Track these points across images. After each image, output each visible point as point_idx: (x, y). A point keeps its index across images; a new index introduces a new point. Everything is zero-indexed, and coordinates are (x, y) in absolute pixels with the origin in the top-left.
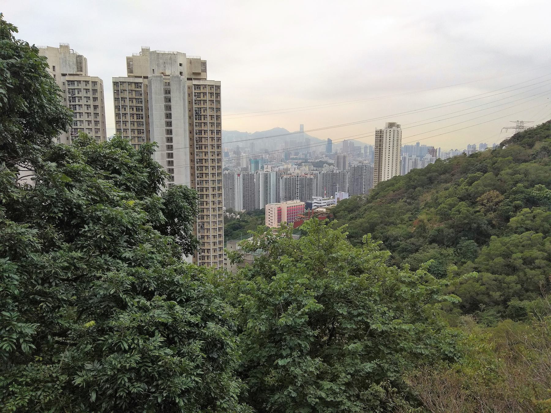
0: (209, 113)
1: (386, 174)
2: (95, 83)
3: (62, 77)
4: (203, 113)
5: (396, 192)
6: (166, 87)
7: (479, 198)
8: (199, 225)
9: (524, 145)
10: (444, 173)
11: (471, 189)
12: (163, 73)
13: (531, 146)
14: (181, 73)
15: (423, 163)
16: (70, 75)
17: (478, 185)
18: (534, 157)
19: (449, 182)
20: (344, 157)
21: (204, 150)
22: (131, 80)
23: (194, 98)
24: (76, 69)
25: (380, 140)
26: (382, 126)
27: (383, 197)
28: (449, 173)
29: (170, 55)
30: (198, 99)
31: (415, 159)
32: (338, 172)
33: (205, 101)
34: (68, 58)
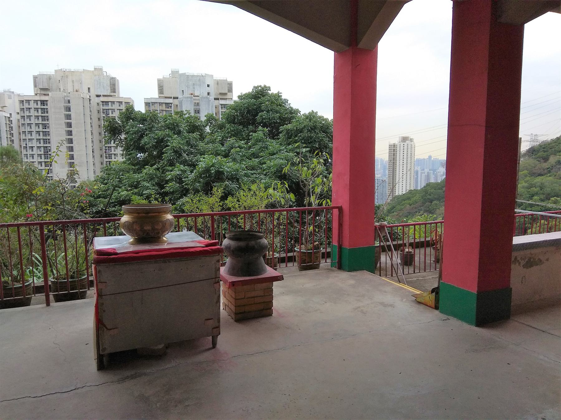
1: (401, 188)
3: (97, 98)
5: (412, 206)
6: (196, 107)
9: (539, 159)
12: (192, 94)
13: (546, 159)
14: (208, 94)
15: (436, 177)
16: (104, 96)
18: (549, 171)
22: (163, 101)
24: (109, 91)
25: (394, 154)
26: (396, 141)
27: (399, 210)
31: (428, 173)
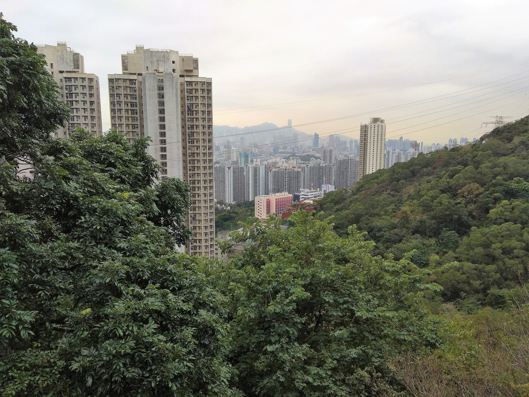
0: (200, 108)
1: (371, 167)
2: (91, 80)
3: (60, 74)
4: (194, 109)
5: (380, 185)
6: (159, 84)
7: (460, 191)
8: (191, 216)
9: (503, 140)
10: (426, 167)
11: (453, 182)
12: (156, 70)
13: (510, 140)
14: (174, 70)
15: (406, 157)
16: (67, 72)
17: (459, 178)
18: (513, 151)
19: (431, 175)
20: (331, 151)
21: (195, 144)
22: (126, 77)
23: (186, 94)
24: (73, 67)
25: (365, 135)
26: (367, 121)
27: (368, 189)
28: (431, 166)
29: (163, 53)
30: (190, 95)
31: (399, 153)
32: (324, 165)
33: (197, 97)
34: (65, 56)
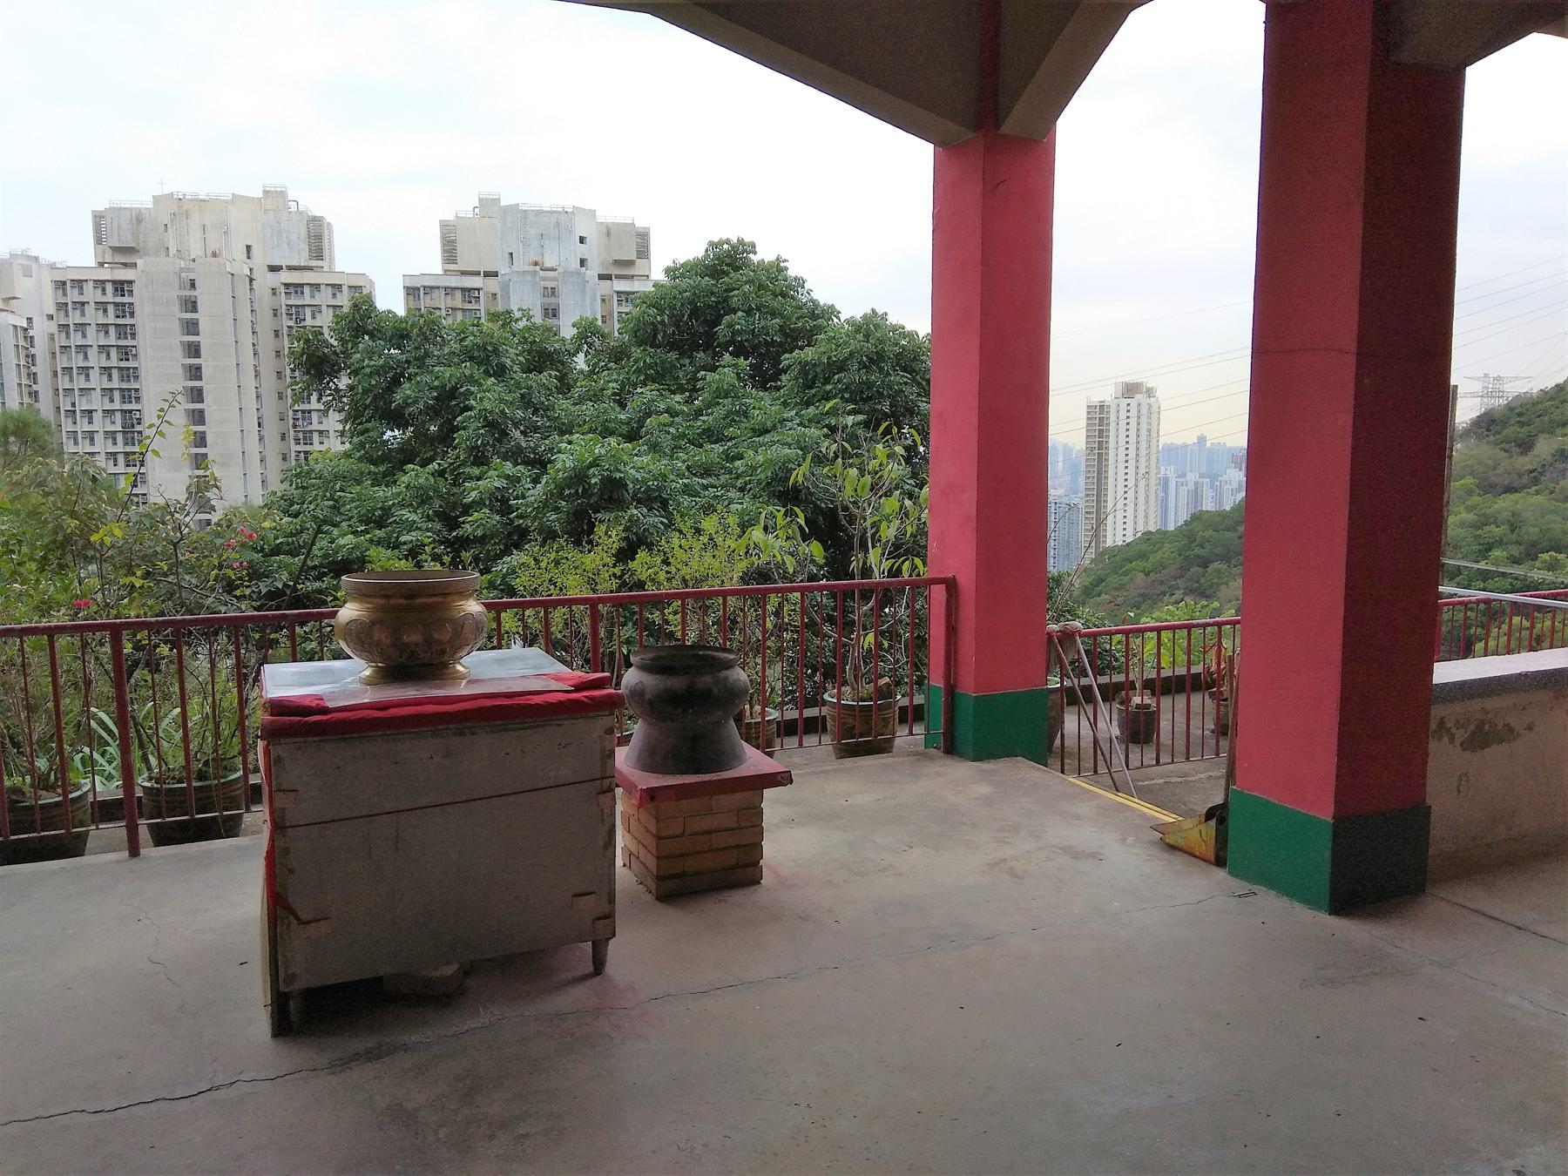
1: (1120, 526)
3: (270, 274)
5: (1153, 576)
6: (547, 300)
9: (1507, 446)
12: (536, 264)
13: (1526, 446)
14: (583, 262)
15: (1219, 497)
16: (290, 268)
18: (1535, 477)
22: (454, 282)
24: (305, 254)
25: (1101, 431)
26: (1106, 394)
27: (1117, 589)
31: (1196, 484)
